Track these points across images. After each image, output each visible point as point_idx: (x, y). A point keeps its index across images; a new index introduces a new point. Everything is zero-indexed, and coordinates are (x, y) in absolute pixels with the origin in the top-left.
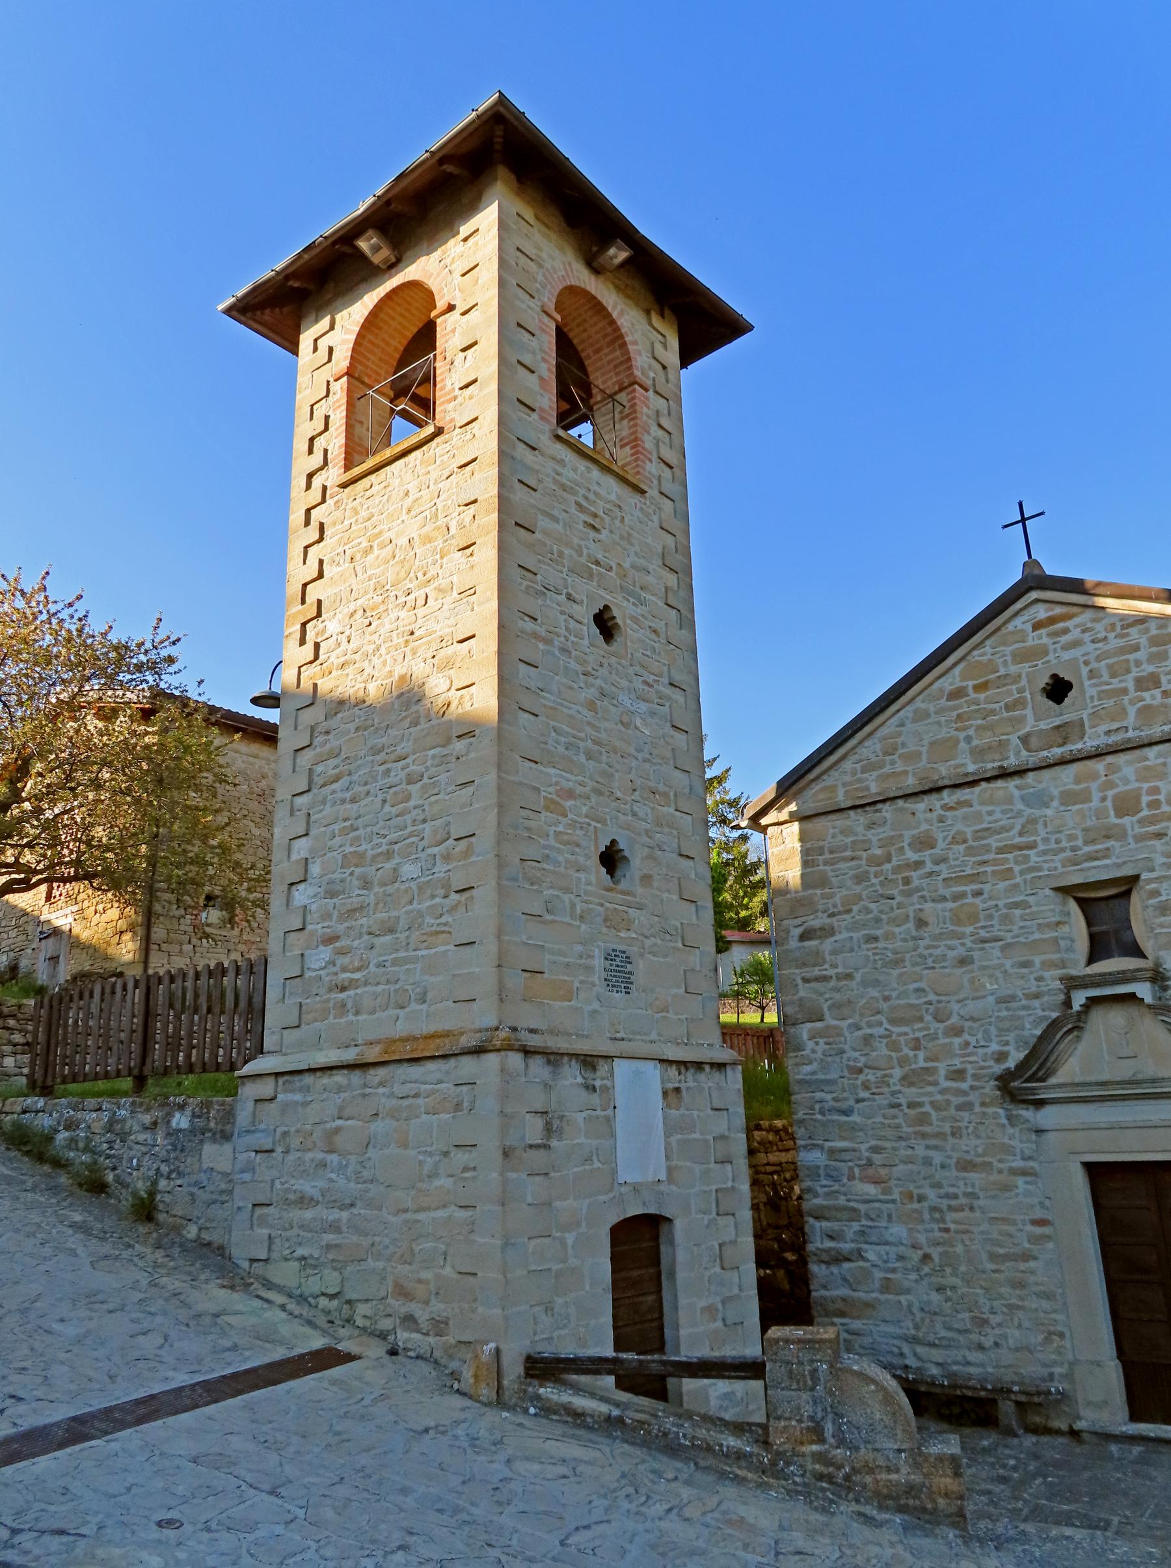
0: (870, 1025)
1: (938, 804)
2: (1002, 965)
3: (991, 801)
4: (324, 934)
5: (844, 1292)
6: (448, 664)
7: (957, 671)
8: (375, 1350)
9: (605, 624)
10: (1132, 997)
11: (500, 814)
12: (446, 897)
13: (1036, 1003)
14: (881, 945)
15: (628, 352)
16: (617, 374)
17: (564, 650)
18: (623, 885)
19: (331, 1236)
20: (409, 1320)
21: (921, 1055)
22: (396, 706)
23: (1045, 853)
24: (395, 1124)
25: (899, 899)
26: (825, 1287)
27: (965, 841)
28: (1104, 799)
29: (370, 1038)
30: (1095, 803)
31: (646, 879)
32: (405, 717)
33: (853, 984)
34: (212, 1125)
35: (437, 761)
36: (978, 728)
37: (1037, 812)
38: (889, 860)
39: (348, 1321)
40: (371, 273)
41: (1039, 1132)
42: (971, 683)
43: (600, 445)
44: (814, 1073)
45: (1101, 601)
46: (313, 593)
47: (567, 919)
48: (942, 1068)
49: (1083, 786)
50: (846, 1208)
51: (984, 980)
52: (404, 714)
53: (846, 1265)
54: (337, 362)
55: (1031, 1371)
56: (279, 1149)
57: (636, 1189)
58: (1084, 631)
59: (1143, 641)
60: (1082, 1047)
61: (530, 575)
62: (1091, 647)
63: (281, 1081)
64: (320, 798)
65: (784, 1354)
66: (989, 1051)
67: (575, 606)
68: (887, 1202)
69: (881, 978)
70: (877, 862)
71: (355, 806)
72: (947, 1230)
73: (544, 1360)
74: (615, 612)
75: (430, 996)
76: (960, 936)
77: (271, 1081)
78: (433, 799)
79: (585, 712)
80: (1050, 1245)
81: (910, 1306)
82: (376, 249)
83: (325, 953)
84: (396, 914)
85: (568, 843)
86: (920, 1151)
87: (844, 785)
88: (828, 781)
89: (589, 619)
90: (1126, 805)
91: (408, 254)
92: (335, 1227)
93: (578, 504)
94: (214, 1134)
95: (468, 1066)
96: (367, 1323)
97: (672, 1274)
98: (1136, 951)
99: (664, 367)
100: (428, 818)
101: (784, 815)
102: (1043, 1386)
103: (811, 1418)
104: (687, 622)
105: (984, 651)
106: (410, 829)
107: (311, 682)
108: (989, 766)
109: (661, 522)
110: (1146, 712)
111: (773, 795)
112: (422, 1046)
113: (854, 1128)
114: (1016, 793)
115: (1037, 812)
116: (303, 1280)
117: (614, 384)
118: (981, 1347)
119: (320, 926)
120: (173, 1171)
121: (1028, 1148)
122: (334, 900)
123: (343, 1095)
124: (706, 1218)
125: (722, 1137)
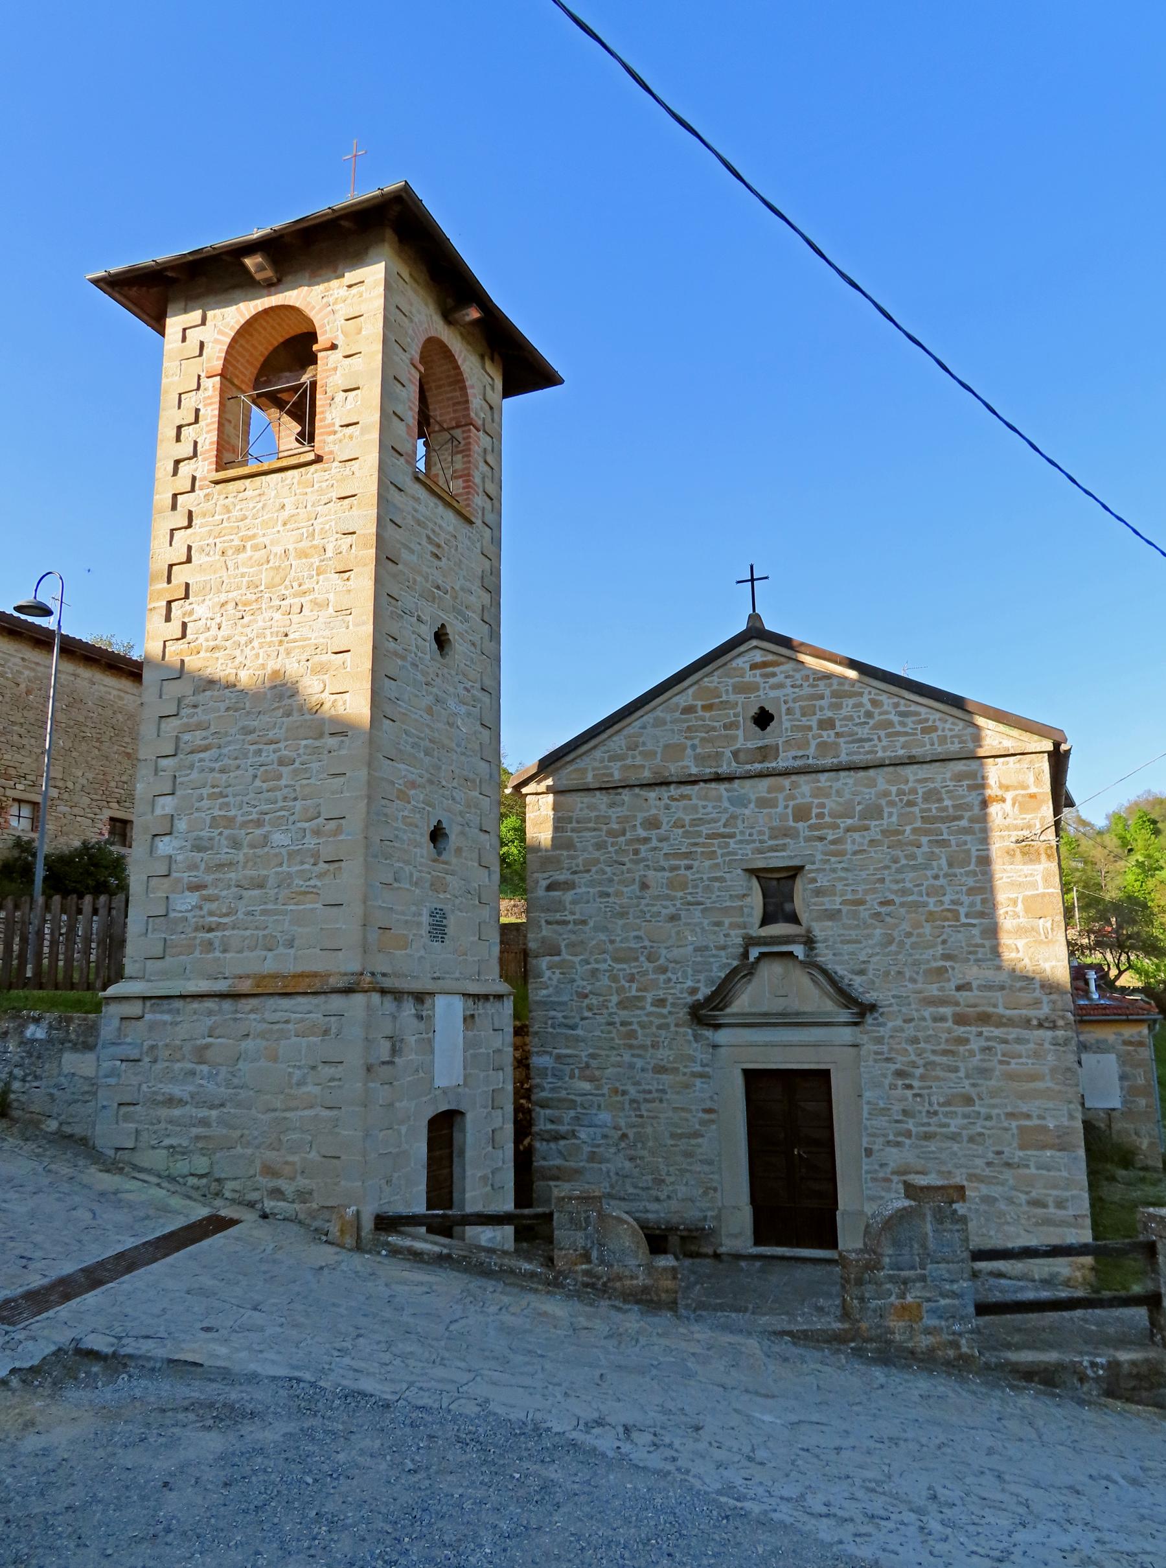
0: (597, 961)
1: (666, 795)
2: (701, 923)
3: (706, 798)
4: (191, 882)
5: (558, 1162)
6: (321, 669)
7: (690, 691)
8: (249, 1216)
9: (441, 639)
10: (790, 954)
11: (368, 804)
12: (314, 865)
13: (723, 953)
14: (611, 900)
15: (466, 395)
16: (455, 411)
17: (415, 665)
18: (444, 857)
19: (200, 1130)
20: (277, 1193)
21: (634, 986)
22: (269, 696)
23: (741, 842)
24: (264, 1043)
25: (629, 865)
26: (544, 1159)
27: (683, 826)
28: (786, 807)
29: (239, 972)
30: (780, 809)
31: (459, 850)
32: (278, 708)
33: (586, 929)
34: (73, 1036)
35: (308, 751)
36: (702, 739)
37: (739, 811)
38: (624, 834)
39: (217, 1194)
40: (247, 285)
41: (715, 1046)
42: (700, 703)
43: (434, 471)
44: (549, 996)
45: (803, 657)
46: (181, 575)
47: (408, 886)
48: (649, 997)
49: (773, 795)
50: (565, 1100)
51: (687, 933)
52: (277, 705)
53: (562, 1143)
54: (209, 360)
55: (692, 1214)
56: (147, 1059)
57: (445, 1091)
58: (786, 677)
59: (827, 693)
60: (750, 988)
61: (393, 602)
62: (789, 690)
63: (148, 1003)
64: (187, 763)
65: (569, 1208)
66: (685, 986)
67: (422, 626)
68: (597, 1095)
69: (609, 926)
70: (611, 833)
71: (224, 776)
72: (641, 1116)
73: (389, 1218)
74: (449, 630)
75: (296, 943)
76: (672, 899)
77: (139, 1003)
78: (305, 782)
79: (425, 716)
80: (714, 1127)
81: (608, 1172)
82: (260, 268)
83: (193, 899)
84: (265, 872)
85: (411, 824)
86: (627, 1058)
87: (594, 769)
88: (580, 764)
89: (430, 637)
90: (801, 814)
91: (289, 278)
92: (204, 1122)
93: (428, 537)
94: (75, 1044)
95: (337, 1002)
96: (236, 1196)
97: (462, 1153)
98: (794, 919)
99: (491, 408)
100: (300, 797)
101: (542, 787)
102: (700, 1225)
103: (584, 1248)
104: (495, 636)
105: (712, 680)
106: (281, 804)
107: (178, 658)
108: (708, 770)
109: (482, 547)
110: (823, 746)
111: (535, 771)
112: (293, 983)
113: (578, 1039)
114: (725, 794)
115: (739, 811)
116: (171, 1165)
117: (451, 419)
118: (657, 1200)
119: (186, 874)
120: (29, 1074)
121: (706, 1057)
122: (201, 854)
123: (214, 1018)
124: (486, 1111)
125: (499, 1051)
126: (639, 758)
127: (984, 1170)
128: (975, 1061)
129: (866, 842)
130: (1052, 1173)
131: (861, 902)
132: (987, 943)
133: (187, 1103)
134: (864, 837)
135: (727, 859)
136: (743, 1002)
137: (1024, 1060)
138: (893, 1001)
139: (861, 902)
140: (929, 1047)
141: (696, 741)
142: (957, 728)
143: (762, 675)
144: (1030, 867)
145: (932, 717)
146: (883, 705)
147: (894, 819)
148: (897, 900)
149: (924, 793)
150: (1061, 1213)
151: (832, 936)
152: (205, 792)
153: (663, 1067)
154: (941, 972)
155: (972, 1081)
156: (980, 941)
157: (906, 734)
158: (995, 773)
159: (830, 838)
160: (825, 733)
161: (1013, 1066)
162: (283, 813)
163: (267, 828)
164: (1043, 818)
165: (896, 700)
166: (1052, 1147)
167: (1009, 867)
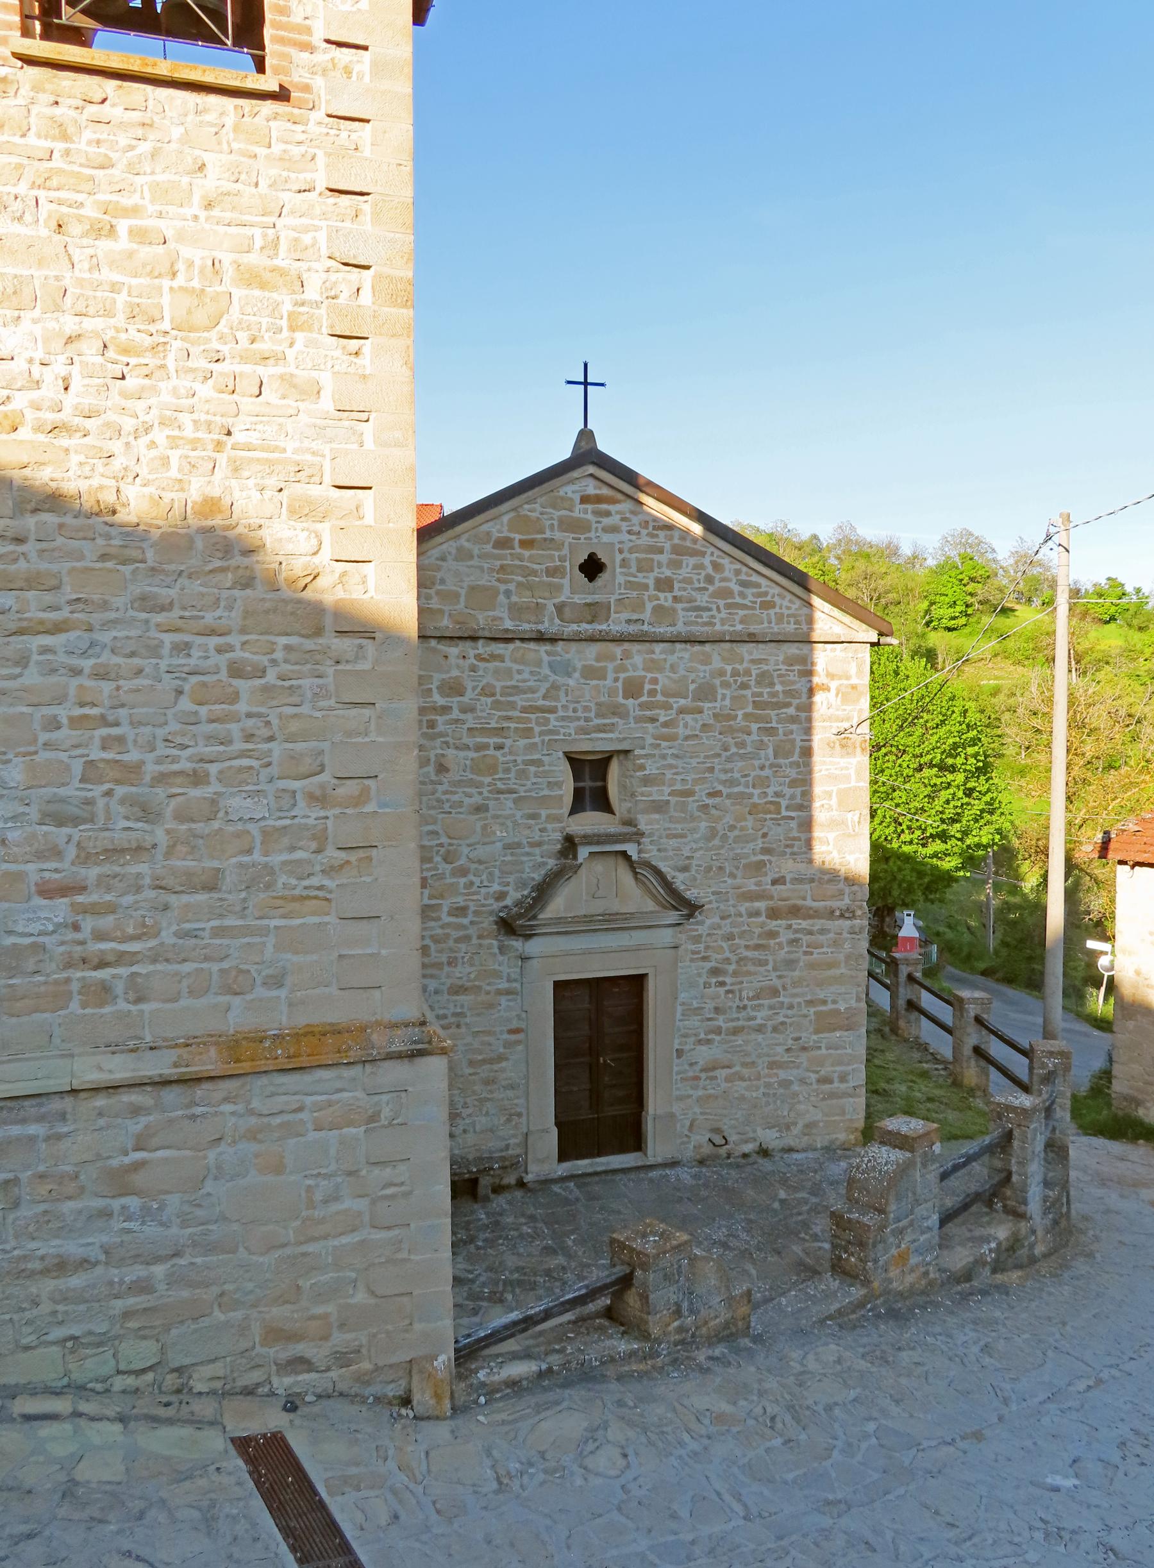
1: (471, 653)
2: (514, 815)
3: (522, 662)
12: (318, 851)
13: (537, 851)
20: (301, 1363)
23: (563, 719)
24: (254, 1147)
27: (493, 695)
30: (609, 682)
32: (223, 570)
36: (519, 584)
37: (561, 680)
41: (524, 959)
42: (518, 537)
51: (496, 828)
52: (218, 563)
59: (667, 546)
66: (491, 890)
71: (107, 687)
75: (289, 980)
76: (479, 785)
80: (520, 1048)
84: (216, 864)
90: (633, 689)
92: (143, 1287)
105: (532, 507)
106: (239, 745)
108: (526, 626)
114: (546, 658)
115: (561, 680)
119: (31, 867)
122: (66, 830)
126: (435, 600)
127: (782, 1057)
128: (782, 954)
129: (698, 726)
130: (839, 1052)
131: (689, 793)
132: (803, 836)
133: (96, 1263)
134: (696, 721)
135: (547, 738)
136: (557, 906)
137: (824, 950)
138: (712, 898)
139: (689, 793)
140: (743, 942)
141: (512, 587)
142: (794, 607)
143: (595, 513)
144: (845, 760)
145: (771, 591)
146: (723, 572)
147: (727, 702)
148: (725, 791)
149: (757, 675)
150: (843, 1086)
151: (658, 830)
152: (63, 713)
153: (462, 987)
154: (760, 865)
155: (778, 973)
156: (796, 835)
157: (744, 607)
158: (823, 659)
159: (662, 719)
160: (661, 595)
161: (815, 956)
162: (245, 762)
163: (214, 787)
164: (861, 710)
165: (738, 566)
166: (841, 1028)
167: (828, 760)
